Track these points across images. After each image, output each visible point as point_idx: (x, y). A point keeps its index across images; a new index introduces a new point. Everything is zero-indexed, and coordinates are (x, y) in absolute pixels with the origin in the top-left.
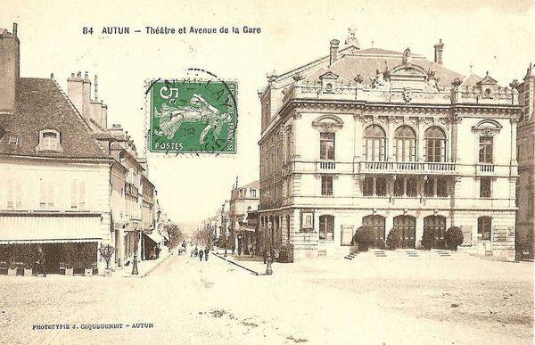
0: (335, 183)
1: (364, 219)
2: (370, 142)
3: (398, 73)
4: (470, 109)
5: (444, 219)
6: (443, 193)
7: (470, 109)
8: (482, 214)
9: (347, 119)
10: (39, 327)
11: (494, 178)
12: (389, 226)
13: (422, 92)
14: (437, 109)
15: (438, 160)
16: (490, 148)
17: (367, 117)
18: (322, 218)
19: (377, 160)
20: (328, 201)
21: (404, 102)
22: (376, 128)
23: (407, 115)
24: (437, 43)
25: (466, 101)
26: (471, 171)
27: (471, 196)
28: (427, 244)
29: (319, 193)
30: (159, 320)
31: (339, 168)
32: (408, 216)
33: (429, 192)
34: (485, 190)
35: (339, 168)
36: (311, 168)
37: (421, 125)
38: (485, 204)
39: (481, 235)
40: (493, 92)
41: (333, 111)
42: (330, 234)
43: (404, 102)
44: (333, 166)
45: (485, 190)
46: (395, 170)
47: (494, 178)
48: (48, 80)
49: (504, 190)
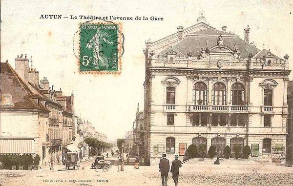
4: (257, 72)
7: (257, 72)
8: (169, 136)
9: (182, 79)
12: (228, 143)
14: (238, 72)
23: (219, 76)
24: (246, 27)
38: (267, 130)
39: (264, 150)
42: (172, 149)
43: (218, 68)
46: (210, 110)
49: (279, 123)
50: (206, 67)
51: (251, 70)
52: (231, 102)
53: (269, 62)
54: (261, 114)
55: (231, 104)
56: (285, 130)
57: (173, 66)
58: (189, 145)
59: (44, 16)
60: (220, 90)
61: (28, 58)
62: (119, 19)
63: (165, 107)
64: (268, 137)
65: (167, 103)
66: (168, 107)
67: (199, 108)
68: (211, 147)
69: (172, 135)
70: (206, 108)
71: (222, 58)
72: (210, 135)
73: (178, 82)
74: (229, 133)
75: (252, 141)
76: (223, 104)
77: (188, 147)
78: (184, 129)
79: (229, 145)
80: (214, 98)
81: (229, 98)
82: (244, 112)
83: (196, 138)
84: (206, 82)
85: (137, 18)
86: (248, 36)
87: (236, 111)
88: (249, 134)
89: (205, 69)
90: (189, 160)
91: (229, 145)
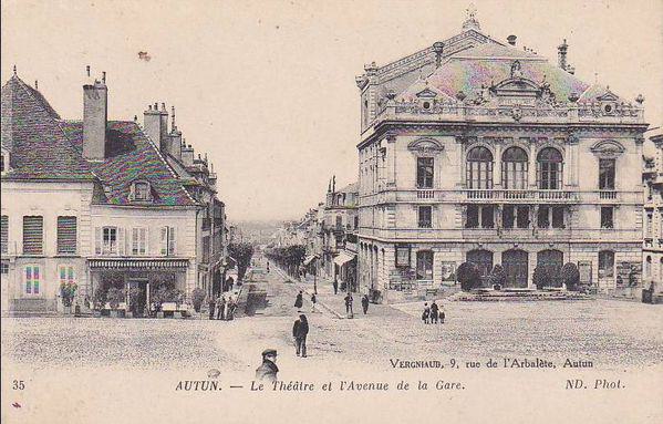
0: (616, 213)
1: (469, 254)
3: (505, 88)
6: (558, 223)
8: (604, 248)
9: (449, 141)
10: (380, 387)
12: (497, 260)
13: (532, 110)
15: (553, 187)
18: (419, 254)
19: (483, 188)
23: (517, 135)
24: (561, 43)
28: (542, 281)
29: (416, 226)
30: (107, 306)
37: (533, 147)
43: (513, 120)
48: (131, 123)
53: (608, 108)
57: (432, 118)
74: (531, 239)
75: (573, 257)
79: (500, 263)
80: (471, 176)
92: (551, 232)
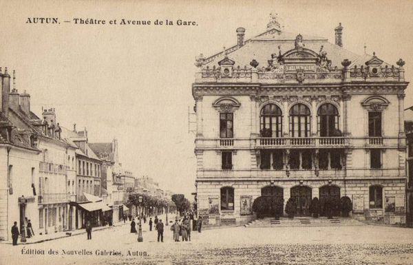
0: (234, 157)
2: (296, 120)
3: (291, 57)
4: (356, 86)
5: (339, 188)
6: (337, 166)
7: (356, 86)
8: (224, 185)
9: (245, 100)
11: (235, 151)
12: (316, 194)
14: (329, 87)
16: (379, 122)
17: (263, 97)
20: (229, 174)
21: (297, 82)
22: (323, 107)
23: (300, 94)
25: (353, 79)
26: (361, 143)
27: (362, 166)
29: (220, 168)
31: (237, 145)
32: (304, 186)
33: (295, 166)
34: (376, 163)
35: (237, 145)
36: (246, 144)
38: (376, 174)
39: (373, 203)
40: (379, 70)
41: (229, 92)
42: (230, 205)
43: (297, 82)
44: (232, 142)
45: (376, 163)
46: (288, 145)
47: (235, 151)
49: (394, 161)
50: (280, 82)
51: (347, 83)
52: (319, 133)
54: (367, 150)
55: (319, 135)
56: (403, 172)
58: (255, 198)
59: (32, 21)
60: (273, 116)
61: (10, 72)
62: (131, 23)
63: (219, 142)
64: (377, 183)
65: (370, 135)
66: (372, 141)
67: (299, 141)
68: (290, 200)
69: (230, 185)
70: (279, 141)
71: (302, 68)
72: (289, 183)
73: (238, 106)
74: (313, 179)
76: (277, 136)
77: (253, 201)
78: (248, 174)
79: (318, 197)
81: (315, 126)
82: (339, 146)
83: (296, 187)
84: (279, 104)
85: (156, 23)
86: (340, 37)
87: (279, 145)
88: (347, 180)
89: (334, 84)
90: (253, 222)
91: (318, 197)
92: (330, 173)
